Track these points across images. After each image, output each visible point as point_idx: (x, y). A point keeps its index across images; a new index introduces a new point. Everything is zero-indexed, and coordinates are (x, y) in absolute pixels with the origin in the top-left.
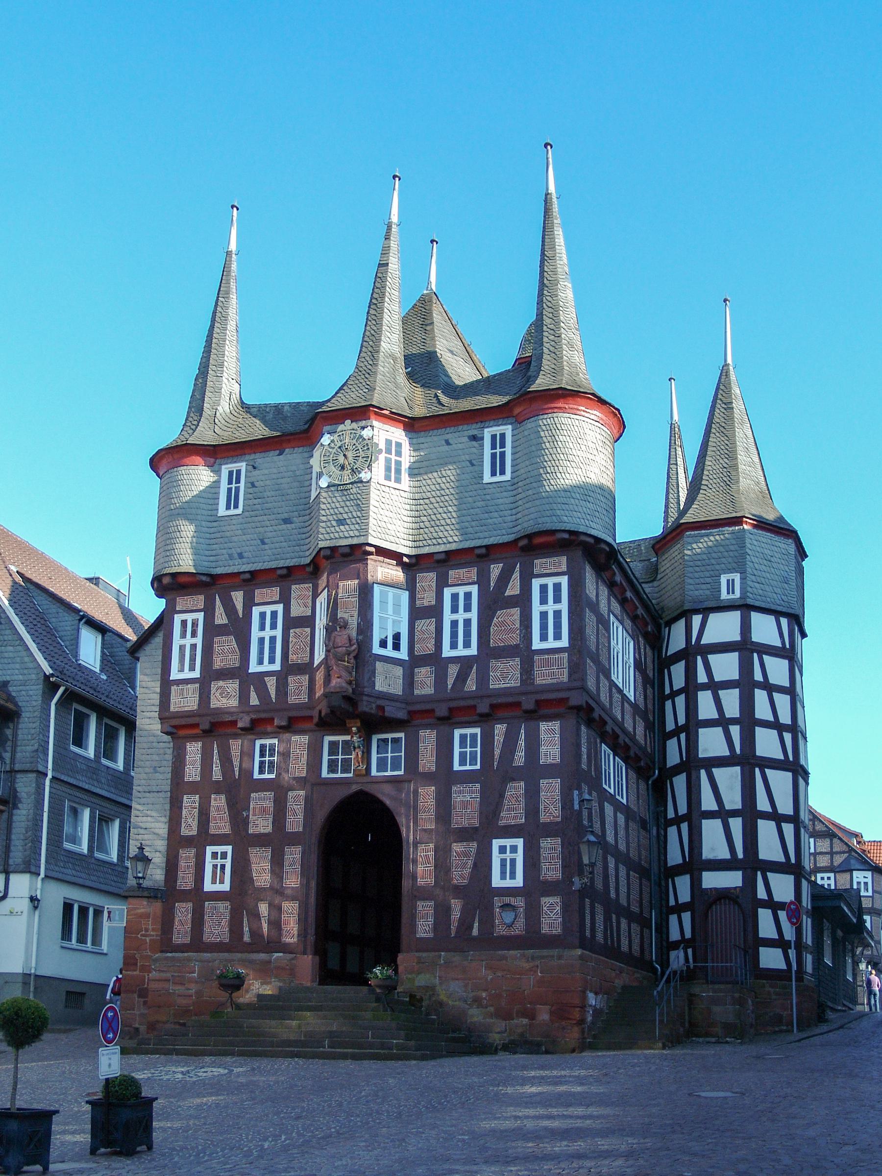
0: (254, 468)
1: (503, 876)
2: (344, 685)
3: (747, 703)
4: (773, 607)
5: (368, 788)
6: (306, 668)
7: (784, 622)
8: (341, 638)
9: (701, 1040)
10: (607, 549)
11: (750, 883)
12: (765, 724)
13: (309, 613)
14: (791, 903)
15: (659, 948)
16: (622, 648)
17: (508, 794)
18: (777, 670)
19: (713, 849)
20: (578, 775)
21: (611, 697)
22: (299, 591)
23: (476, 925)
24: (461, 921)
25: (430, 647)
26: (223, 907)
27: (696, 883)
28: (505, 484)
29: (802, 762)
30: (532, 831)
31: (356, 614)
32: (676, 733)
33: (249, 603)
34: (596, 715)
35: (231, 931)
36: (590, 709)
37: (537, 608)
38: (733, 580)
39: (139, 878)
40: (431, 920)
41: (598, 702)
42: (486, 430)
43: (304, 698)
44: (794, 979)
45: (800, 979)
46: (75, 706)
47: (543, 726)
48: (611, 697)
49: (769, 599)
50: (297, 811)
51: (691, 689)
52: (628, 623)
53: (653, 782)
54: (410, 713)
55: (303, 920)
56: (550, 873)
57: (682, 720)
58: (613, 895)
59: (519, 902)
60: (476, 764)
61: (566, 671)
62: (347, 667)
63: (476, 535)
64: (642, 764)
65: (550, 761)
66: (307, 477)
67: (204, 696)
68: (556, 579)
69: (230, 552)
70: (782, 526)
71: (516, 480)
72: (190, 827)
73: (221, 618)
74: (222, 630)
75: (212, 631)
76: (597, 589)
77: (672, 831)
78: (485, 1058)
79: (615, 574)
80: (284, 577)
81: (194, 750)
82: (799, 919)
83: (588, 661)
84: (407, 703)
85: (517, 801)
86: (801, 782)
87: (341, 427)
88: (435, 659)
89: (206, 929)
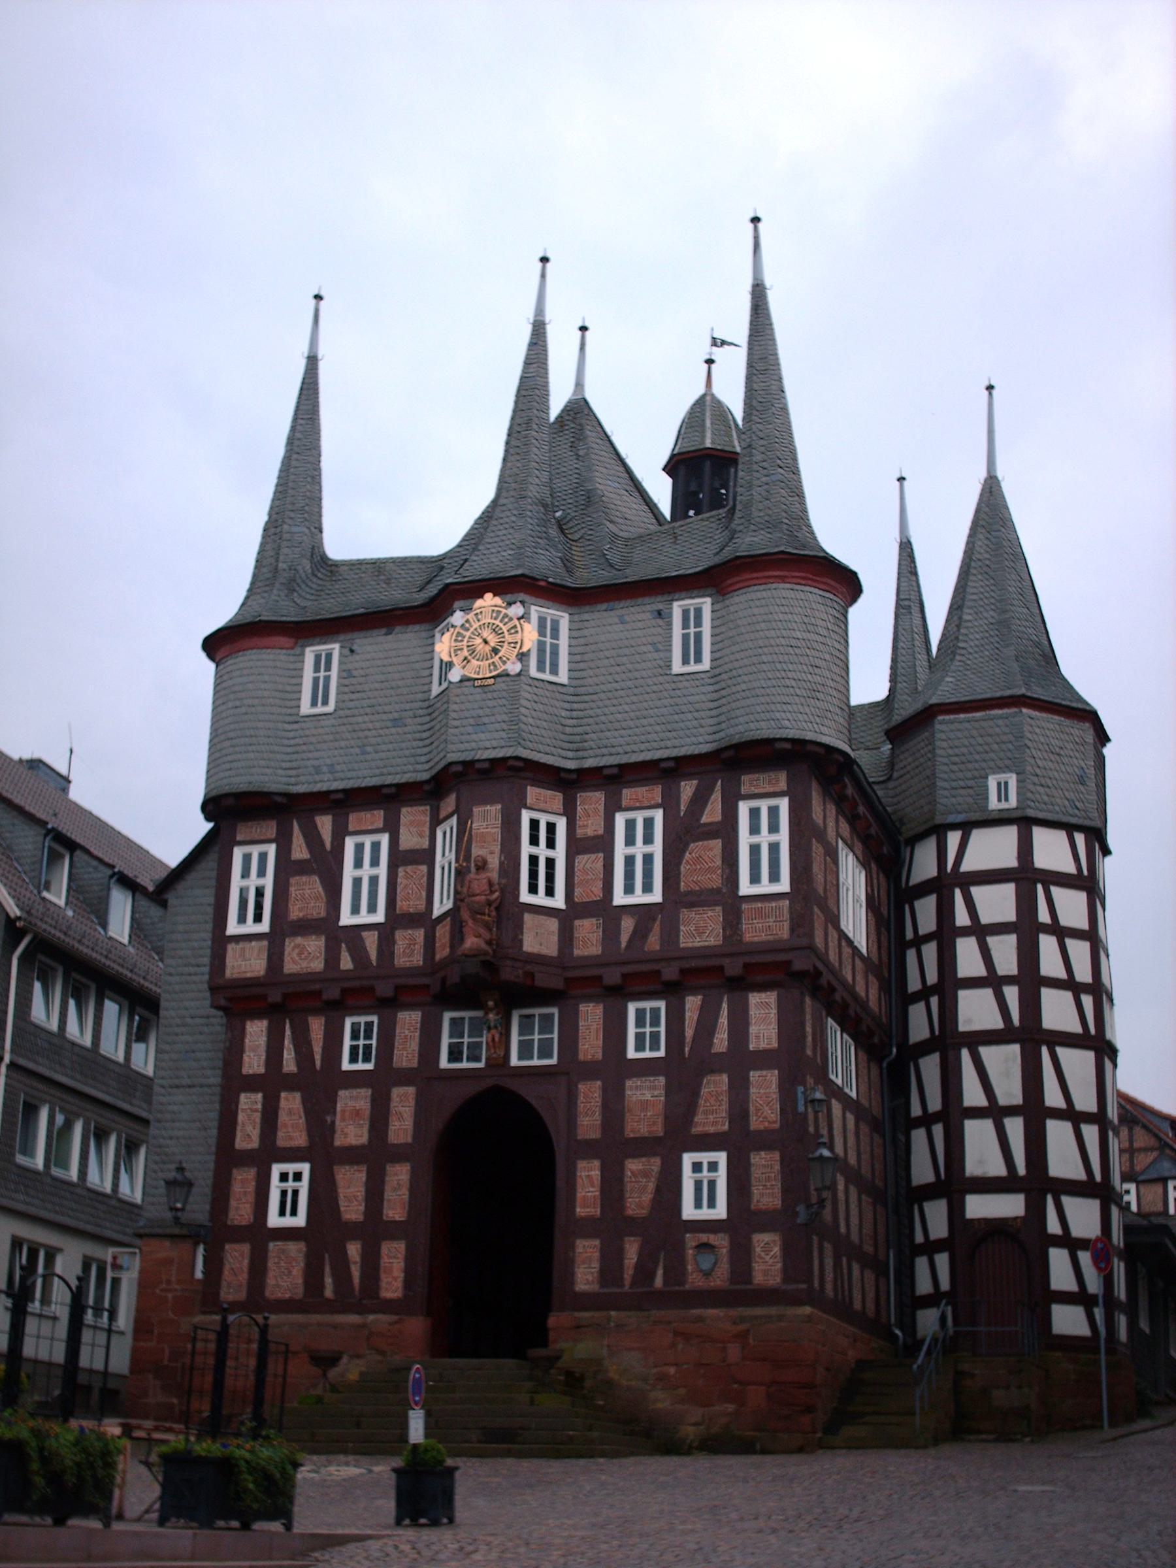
0: (352, 651)
1: (698, 1205)
2: (484, 946)
3: (1029, 955)
4: (1065, 819)
5: (509, 1083)
6: (422, 919)
7: (1080, 838)
8: (478, 882)
9: (972, 1437)
10: (841, 759)
11: (1036, 1211)
12: (1057, 1114)
13: (425, 844)
14: (1097, 1240)
15: (900, 1305)
16: (853, 880)
17: (704, 1091)
18: (1071, 906)
19: (981, 1162)
20: (798, 1063)
21: (840, 953)
22: (412, 817)
23: (660, 1272)
24: (639, 1266)
25: (597, 892)
26: (296, 1249)
27: (956, 1211)
28: (703, 675)
29: (1108, 1036)
30: (739, 1142)
31: (497, 849)
32: (924, 994)
33: (340, 835)
34: (823, 981)
35: (306, 1282)
36: (818, 974)
37: (745, 839)
38: (1006, 783)
39: (177, 1210)
40: (596, 1265)
41: (827, 963)
42: (675, 604)
43: (417, 959)
44: (1103, 1350)
45: (1110, 1351)
46: (41, 957)
47: (754, 999)
48: (840, 953)
49: (1057, 808)
50: (405, 1116)
51: (946, 935)
52: (859, 846)
53: (889, 1065)
54: (568, 981)
55: (409, 1271)
56: (765, 1200)
57: (932, 977)
58: (843, 1230)
59: (721, 1241)
60: (658, 1049)
61: (786, 925)
62: (487, 922)
63: (662, 744)
64: (876, 1040)
65: (763, 1045)
66: (427, 664)
67: (275, 959)
68: (773, 802)
69: (316, 763)
70: (1074, 705)
71: (717, 671)
72: (248, 1136)
73: (299, 851)
74: (302, 868)
75: (286, 869)
76: (824, 810)
77: (919, 1136)
78: (673, 1461)
79: (845, 786)
80: (387, 799)
81: (256, 1032)
82: (1109, 1262)
83: (816, 909)
84: (564, 968)
85: (717, 1100)
86: (1108, 1064)
87: (479, 603)
88: (603, 908)
89: (270, 1281)
